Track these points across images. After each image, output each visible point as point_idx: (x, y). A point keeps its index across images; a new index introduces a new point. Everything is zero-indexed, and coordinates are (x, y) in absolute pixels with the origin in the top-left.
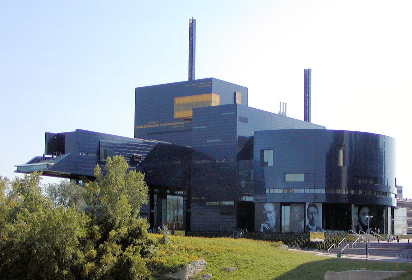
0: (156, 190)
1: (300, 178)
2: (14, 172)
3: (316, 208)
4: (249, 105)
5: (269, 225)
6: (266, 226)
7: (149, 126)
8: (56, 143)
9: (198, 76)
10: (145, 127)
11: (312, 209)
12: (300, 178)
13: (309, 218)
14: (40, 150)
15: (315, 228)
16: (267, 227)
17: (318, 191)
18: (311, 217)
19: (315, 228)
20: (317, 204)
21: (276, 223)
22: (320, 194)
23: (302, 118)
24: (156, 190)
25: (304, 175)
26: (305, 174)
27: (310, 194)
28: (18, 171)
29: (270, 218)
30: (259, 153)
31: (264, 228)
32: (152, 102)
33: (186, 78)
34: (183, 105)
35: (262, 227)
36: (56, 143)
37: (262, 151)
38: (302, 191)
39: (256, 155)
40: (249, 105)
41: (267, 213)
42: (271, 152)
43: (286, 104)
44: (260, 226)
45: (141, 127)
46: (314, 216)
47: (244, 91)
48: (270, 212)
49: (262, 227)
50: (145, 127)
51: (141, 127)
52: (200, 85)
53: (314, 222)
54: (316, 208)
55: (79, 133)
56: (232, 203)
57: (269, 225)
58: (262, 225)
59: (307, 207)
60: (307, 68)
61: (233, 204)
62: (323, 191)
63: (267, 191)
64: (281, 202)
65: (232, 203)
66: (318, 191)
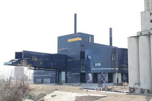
0: (57, 70)
1: (99, 64)
2: (6, 64)
3: (105, 74)
4: (94, 42)
6: (89, 81)
8: (18, 55)
9: (77, 32)
11: (104, 75)
12: (99, 64)
14: (13, 57)
15: (105, 81)
19: (105, 81)
20: (106, 73)
23: (109, 45)
24: (57, 70)
26: (101, 63)
30: (86, 56)
32: (62, 40)
33: (73, 33)
34: (91, 40)
37: (88, 56)
38: (100, 69)
39: (86, 57)
40: (94, 42)
47: (92, 37)
54: (105, 74)
55: (24, 51)
62: (118, 69)
65: (79, 74)
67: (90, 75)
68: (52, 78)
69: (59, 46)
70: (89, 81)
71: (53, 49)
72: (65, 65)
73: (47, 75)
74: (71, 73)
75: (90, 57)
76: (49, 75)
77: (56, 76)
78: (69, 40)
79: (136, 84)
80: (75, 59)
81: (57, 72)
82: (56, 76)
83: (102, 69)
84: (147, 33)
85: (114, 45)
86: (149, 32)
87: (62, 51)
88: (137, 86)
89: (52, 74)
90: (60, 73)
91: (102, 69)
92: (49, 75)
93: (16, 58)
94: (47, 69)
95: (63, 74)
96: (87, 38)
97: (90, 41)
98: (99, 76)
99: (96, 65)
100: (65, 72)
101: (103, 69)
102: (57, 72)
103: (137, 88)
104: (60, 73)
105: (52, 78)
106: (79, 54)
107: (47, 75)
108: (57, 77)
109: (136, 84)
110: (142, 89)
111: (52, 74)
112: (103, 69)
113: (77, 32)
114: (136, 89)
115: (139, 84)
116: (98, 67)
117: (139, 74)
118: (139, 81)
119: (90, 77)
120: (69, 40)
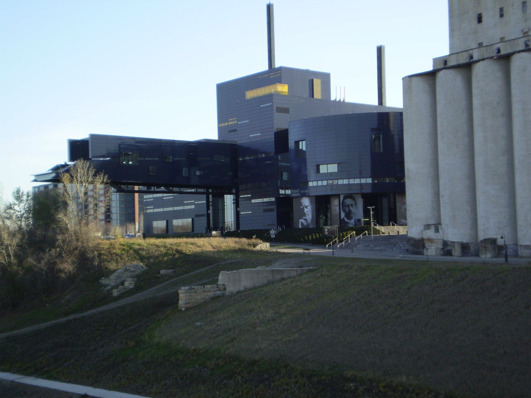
0: (210, 191)
1: (333, 168)
5: (306, 220)
6: (303, 221)
7: (230, 123)
8: (78, 149)
10: (226, 124)
11: (348, 201)
12: (333, 168)
13: (344, 211)
16: (305, 223)
17: (363, 181)
18: (347, 210)
20: (354, 196)
21: (312, 218)
22: (366, 184)
23: (374, 101)
25: (336, 165)
26: (338, 164)
27: (343, 185)
28: (35, 181)
29: (307, 213)
31: (302, 224)
32: (231, 95)
33: (265, 67)
35: (300, 224)
36: (78, 149)
37: (297, 143)
39: (291, 145)
41: (304, 208)
42: (304, 142)
43: (345, 88)
44: (299, 222)
45: (223, 125)
46: (351, 208)
47: (325, 78)
48: (306, 207)
49: (300, 224)
50: (226, 124)
51: (223, 125)
52: (271, 75)
53: (352, 215)
54: (354, 199)
56: (273, 199)
57: (306, 220)
58: (301, 221)
59: (342, 199)
60: (379, 44)
61: (274, 200)
63: (311, 184)
64: (316, 196)
65: (273, 199)
66: (363, 181)
67: (306, 201)
68: (197, 216)
69: (222, 116)
70: (303, 221)
71: (197, 123)
72: (230, 173)
73: (182, 208)
74: (250, 199)
75: (303, 146)
76: (186, 207)
77: (208, 209)
78: (250, 94)
79: (427, 227)
80: (261, 153)
81: (211, 196)
82: (208, 209)
83: (340, 182)
84: (463, 59)
85: (278, 64)
86: (471, 57)
87: (230, 129)
88: (430, 233)
89: (196, 205)
90: (220, 201)
91: (340, 182)
92: (186, 207)
93: (73, 156)
94: (175, 189)
95: (229, 199)
96: (310, 82)
97: (318, 94)
98: (335, 203)
99: (323, 169)
100: (232, 196)
101: (345, 182)
102: (211, 196)
103: (430, 240)
104: (220, 201)
105: (197, 216)
106: (271, 137)
107: (182, 208)
108: (210, 212)
109: (427, 227)
110: (445, 243)
111: (196, 205)
112: (345, 182)
113: (278, 64)
114: (427, 244)
115: (437, 227)
116: (329, 176)
117: (437, 194)
118: (439, 216)
119: (306, 210)
120: (250, 94)
